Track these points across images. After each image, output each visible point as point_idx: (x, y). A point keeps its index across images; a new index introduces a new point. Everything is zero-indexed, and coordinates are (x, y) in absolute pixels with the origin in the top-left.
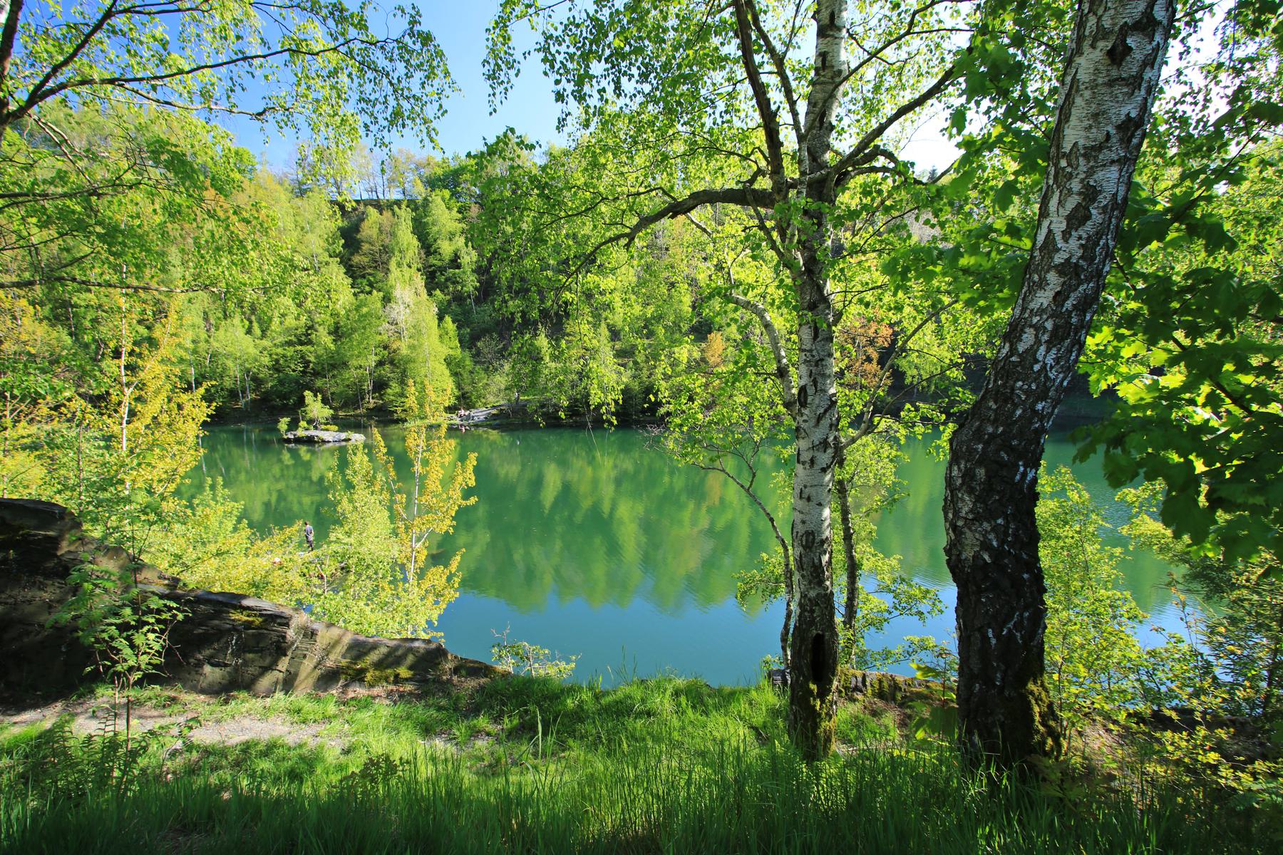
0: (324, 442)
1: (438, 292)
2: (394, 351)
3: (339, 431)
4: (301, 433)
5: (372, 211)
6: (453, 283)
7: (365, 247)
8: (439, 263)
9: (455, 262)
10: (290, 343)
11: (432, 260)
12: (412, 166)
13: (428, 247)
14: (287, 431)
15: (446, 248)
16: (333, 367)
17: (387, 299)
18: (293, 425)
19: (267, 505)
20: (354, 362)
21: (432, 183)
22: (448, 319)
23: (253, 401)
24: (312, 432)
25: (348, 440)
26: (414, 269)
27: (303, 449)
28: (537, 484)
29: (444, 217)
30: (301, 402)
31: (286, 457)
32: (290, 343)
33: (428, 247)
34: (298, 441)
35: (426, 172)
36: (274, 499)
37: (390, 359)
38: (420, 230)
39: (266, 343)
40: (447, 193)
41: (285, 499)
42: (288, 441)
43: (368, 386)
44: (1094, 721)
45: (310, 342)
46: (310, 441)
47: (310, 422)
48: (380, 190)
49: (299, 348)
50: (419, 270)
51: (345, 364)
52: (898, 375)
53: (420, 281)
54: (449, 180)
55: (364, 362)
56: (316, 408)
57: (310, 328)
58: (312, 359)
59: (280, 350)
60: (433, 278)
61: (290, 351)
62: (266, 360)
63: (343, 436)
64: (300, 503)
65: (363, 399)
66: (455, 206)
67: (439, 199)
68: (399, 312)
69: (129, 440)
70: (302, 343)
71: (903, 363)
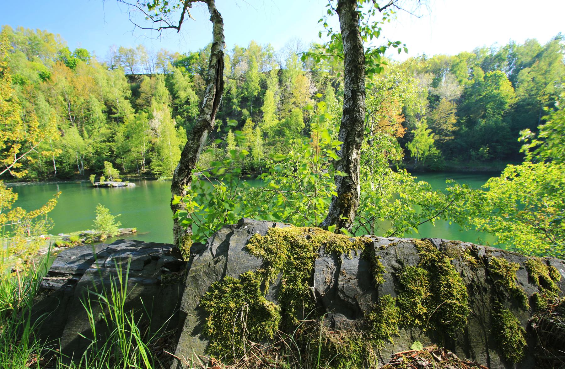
0: (113, 187)
1: (179, 117)
2: (154, 144)
5: (147, 78)
6: (187, 112)
7: (143, 95)
8: (180, 103)
9: (187, 102)
10: (104, 141)
11: (177, 101)
12: (168, 57)
13: (174, 95)
14: (95, 182)
15: (183, 95)
16: (125, 152)
17: (150, 117)
18: (97, 179)
20: (133, 149)
21: (176, 65)
22: (181, 128)
23: (86, 170)
26: (167, 105)
27: (103, 190)
29: (182, 80)
30: (103, 167)
32: (104, 141)
33: (174, 95)
34: (100, 186)
35: (174, 60)
37: (153, 149)
38: (170, 86)
39: (91, 141)
40: (184, 69)
42: (96, 187)
43: (143, 162)
44: (127, 137)
45: (114, 141)
46: (106, 186)
48: (152, 69)
49: (108, 144)
50: (169, 106)
51: (130, 150)
52: (407, 152)
53: (168, 111)
56: (109, 169)
57: (113, 134)
58: (115, 149)
59: (98, 145)
60: (176, 111)
61: (104, 145)
62: (91, 150)
63: (124, 184)
65: (140, 169)
66: (187, 75)
67: (179, 72)
68: (156, 123)
70: (109, 141)
71: (410, 146)
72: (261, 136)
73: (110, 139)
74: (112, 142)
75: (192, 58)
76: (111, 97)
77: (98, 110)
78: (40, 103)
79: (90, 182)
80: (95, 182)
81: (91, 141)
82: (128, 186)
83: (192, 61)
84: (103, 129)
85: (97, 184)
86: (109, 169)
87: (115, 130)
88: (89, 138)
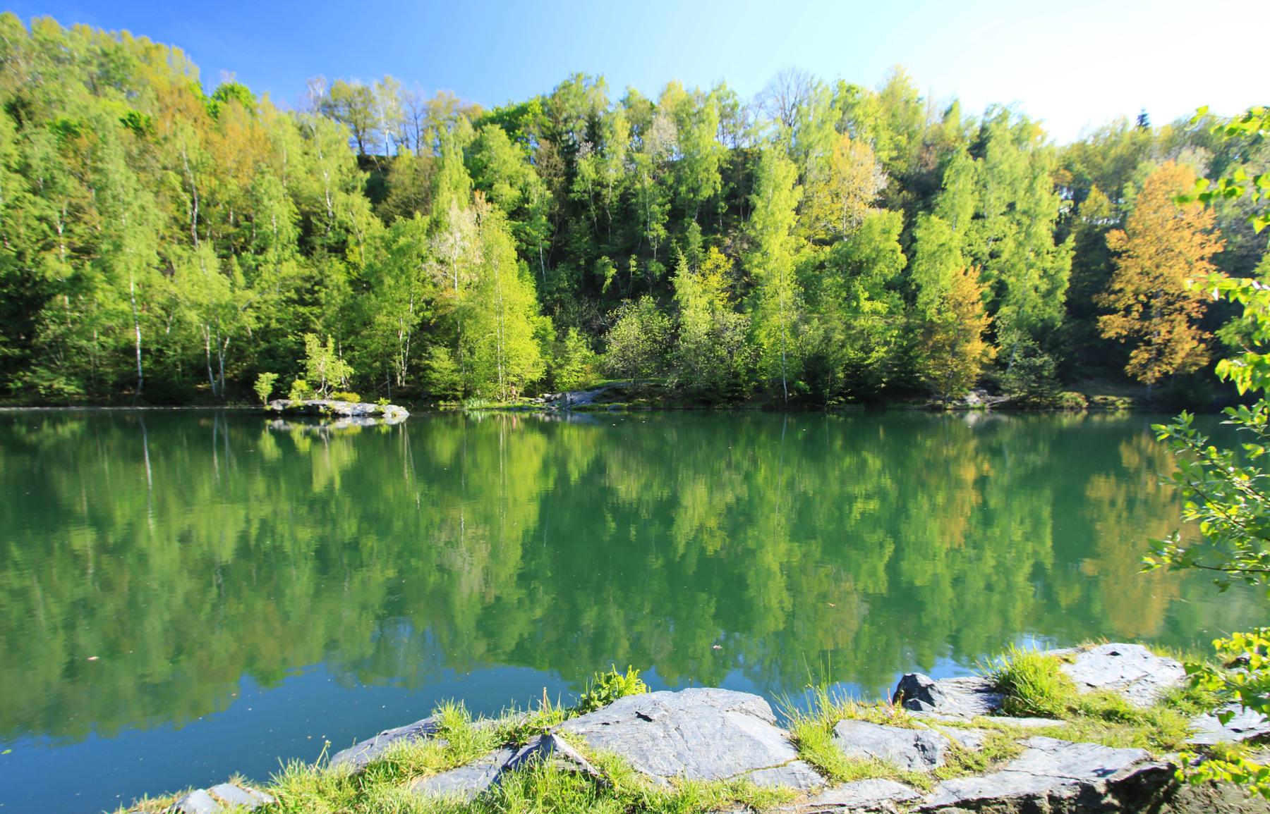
0: (336, 416)
3: (363, 401)
4: (295, 400)
10: (290, 301)
14: (272, 397)
18: (279, 391)
19: (244, 537)
24: (316, 400)
25: (379, 415)
28: (667, 510)
30: (300, 353)
31: (268, 444)
34: (291, 414)
36: (254, 531)
39: (252, 295)
41: (273, 534)
42: (273, 415)
45: (316, 303)
46: (310, 414)
47: (316, 386)
49: (301, 309)
54: (511, 122)
55: (396, 319)
56: (325, 362)
57: (316, 284)
64: (295, 540)
67: (497, 135)
69: (426, 725)
70: (302, 302)
72: (1207, 166)
73: (307, 297)
74: (313, 304)
75: (523, 110)
76: (310, 187)
77: (280, 218)
78: (110, 167)
79: (254, 397)
80: (272, 397)
81: (252, 295)
82: (388, 415)
83: (523, 119)
84: (287, 266)
85: (277, 406)
86: (325, 362)
87: (321, 272)
88: (250, 286)
